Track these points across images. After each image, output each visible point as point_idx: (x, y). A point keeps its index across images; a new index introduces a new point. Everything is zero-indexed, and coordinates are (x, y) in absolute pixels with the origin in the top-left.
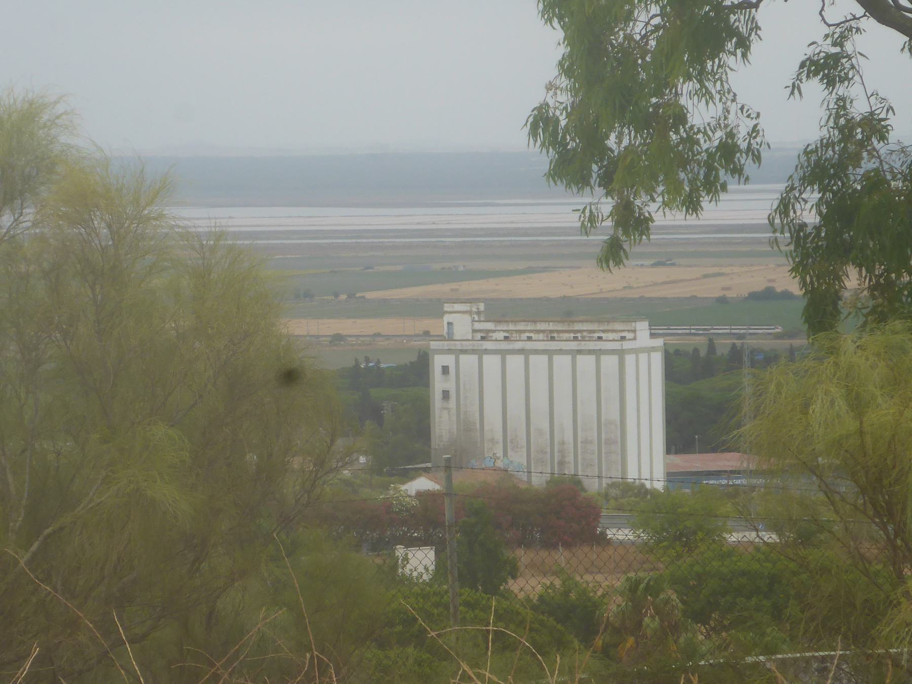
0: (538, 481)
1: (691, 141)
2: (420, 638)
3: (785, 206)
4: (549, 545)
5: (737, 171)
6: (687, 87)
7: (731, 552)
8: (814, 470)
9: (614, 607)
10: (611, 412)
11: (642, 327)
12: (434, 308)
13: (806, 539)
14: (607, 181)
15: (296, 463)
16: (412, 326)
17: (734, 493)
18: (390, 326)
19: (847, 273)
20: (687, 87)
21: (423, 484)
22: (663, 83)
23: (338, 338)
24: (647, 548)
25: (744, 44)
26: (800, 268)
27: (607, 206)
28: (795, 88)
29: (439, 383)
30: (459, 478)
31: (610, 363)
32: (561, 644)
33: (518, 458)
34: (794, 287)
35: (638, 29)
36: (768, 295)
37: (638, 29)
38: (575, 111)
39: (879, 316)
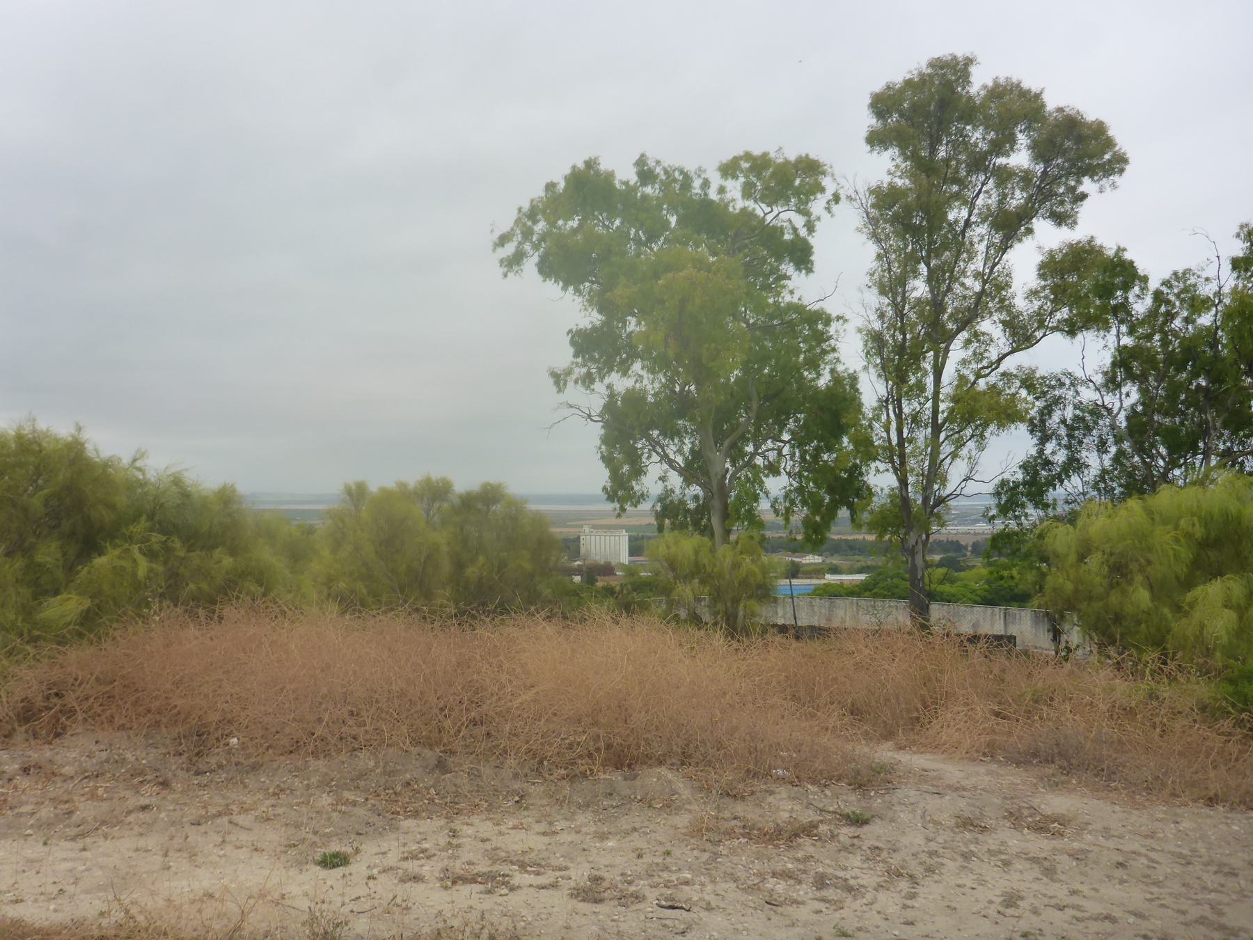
0: (602, 563)
1: (635, 493)
2: (577, 595)
3: (653, 506)
4: (604, 576)
5: (644, 500)
6: (634, 483)
7: (641, 577)
8: (658, 560)
9: (618, 589)
10: (617, 548)
11: (624, 531)
12: (581, 526)
13: (657, 575)
14: (618, 501)
15: (553, 558)
16: (578, 530)
17: (642, 565)
18: (573, 530)
19: (1022, 349)
20: (634, 483)
21: (578, 563)
22: (629, 481)
23: (561, 532)
24: (625, 576)
25: (645, 474)
26: (657, 519)
27: (618, 506)
28: (656, 482)
29: (582, 542)
30: (586, 562)
31: (617, 538)
32: (607, 596)
33: (598, 558)
34: (655, 523)
35: (624, 470)
36: (649, 524)
37: (624, 470)
38: (611, 487)
39: (672, 529)
